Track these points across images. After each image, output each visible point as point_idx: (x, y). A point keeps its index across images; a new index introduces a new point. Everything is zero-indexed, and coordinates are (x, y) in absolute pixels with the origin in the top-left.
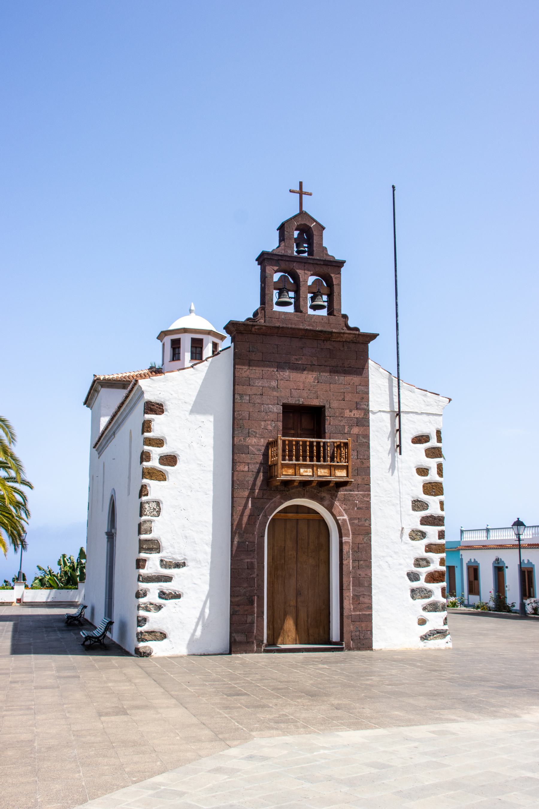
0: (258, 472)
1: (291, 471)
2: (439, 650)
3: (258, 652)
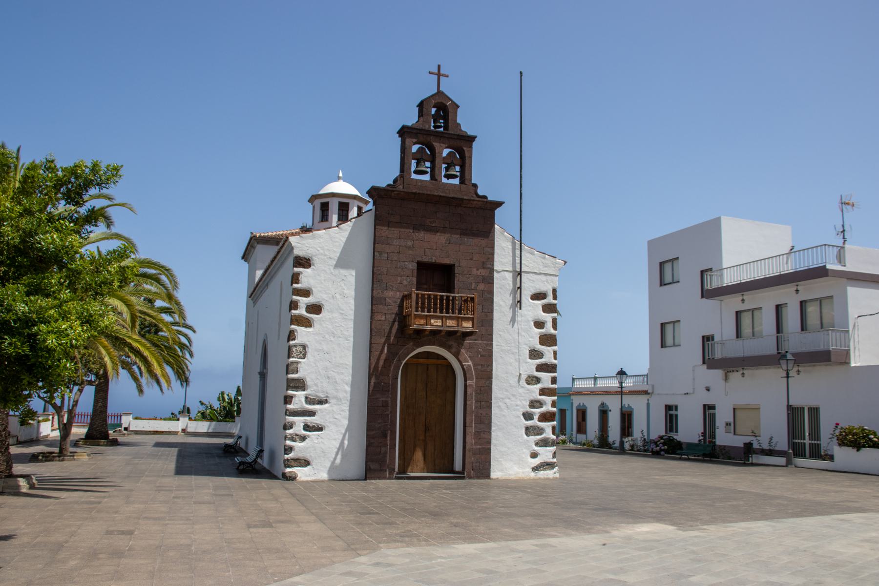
0: (394, 321)
1: (423, 321)
2: (548, 479)
3: (390, 478)
